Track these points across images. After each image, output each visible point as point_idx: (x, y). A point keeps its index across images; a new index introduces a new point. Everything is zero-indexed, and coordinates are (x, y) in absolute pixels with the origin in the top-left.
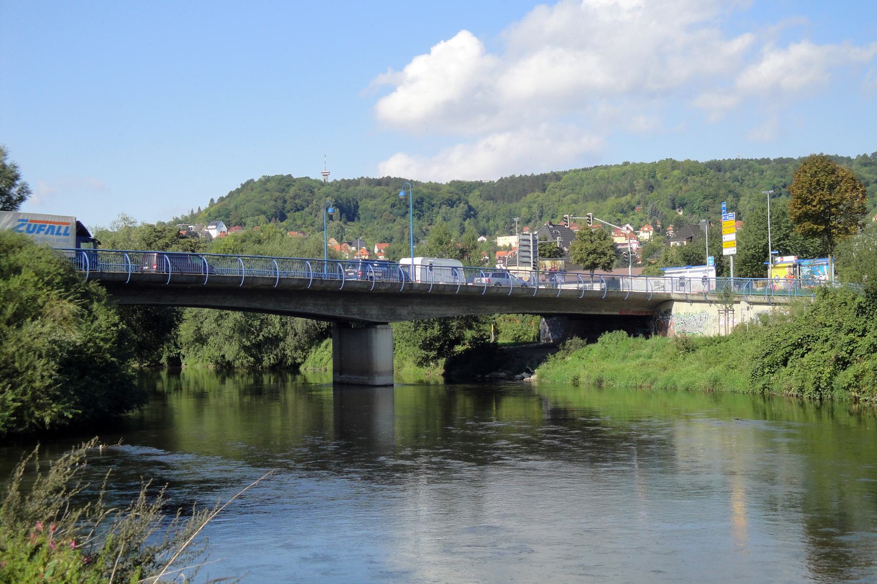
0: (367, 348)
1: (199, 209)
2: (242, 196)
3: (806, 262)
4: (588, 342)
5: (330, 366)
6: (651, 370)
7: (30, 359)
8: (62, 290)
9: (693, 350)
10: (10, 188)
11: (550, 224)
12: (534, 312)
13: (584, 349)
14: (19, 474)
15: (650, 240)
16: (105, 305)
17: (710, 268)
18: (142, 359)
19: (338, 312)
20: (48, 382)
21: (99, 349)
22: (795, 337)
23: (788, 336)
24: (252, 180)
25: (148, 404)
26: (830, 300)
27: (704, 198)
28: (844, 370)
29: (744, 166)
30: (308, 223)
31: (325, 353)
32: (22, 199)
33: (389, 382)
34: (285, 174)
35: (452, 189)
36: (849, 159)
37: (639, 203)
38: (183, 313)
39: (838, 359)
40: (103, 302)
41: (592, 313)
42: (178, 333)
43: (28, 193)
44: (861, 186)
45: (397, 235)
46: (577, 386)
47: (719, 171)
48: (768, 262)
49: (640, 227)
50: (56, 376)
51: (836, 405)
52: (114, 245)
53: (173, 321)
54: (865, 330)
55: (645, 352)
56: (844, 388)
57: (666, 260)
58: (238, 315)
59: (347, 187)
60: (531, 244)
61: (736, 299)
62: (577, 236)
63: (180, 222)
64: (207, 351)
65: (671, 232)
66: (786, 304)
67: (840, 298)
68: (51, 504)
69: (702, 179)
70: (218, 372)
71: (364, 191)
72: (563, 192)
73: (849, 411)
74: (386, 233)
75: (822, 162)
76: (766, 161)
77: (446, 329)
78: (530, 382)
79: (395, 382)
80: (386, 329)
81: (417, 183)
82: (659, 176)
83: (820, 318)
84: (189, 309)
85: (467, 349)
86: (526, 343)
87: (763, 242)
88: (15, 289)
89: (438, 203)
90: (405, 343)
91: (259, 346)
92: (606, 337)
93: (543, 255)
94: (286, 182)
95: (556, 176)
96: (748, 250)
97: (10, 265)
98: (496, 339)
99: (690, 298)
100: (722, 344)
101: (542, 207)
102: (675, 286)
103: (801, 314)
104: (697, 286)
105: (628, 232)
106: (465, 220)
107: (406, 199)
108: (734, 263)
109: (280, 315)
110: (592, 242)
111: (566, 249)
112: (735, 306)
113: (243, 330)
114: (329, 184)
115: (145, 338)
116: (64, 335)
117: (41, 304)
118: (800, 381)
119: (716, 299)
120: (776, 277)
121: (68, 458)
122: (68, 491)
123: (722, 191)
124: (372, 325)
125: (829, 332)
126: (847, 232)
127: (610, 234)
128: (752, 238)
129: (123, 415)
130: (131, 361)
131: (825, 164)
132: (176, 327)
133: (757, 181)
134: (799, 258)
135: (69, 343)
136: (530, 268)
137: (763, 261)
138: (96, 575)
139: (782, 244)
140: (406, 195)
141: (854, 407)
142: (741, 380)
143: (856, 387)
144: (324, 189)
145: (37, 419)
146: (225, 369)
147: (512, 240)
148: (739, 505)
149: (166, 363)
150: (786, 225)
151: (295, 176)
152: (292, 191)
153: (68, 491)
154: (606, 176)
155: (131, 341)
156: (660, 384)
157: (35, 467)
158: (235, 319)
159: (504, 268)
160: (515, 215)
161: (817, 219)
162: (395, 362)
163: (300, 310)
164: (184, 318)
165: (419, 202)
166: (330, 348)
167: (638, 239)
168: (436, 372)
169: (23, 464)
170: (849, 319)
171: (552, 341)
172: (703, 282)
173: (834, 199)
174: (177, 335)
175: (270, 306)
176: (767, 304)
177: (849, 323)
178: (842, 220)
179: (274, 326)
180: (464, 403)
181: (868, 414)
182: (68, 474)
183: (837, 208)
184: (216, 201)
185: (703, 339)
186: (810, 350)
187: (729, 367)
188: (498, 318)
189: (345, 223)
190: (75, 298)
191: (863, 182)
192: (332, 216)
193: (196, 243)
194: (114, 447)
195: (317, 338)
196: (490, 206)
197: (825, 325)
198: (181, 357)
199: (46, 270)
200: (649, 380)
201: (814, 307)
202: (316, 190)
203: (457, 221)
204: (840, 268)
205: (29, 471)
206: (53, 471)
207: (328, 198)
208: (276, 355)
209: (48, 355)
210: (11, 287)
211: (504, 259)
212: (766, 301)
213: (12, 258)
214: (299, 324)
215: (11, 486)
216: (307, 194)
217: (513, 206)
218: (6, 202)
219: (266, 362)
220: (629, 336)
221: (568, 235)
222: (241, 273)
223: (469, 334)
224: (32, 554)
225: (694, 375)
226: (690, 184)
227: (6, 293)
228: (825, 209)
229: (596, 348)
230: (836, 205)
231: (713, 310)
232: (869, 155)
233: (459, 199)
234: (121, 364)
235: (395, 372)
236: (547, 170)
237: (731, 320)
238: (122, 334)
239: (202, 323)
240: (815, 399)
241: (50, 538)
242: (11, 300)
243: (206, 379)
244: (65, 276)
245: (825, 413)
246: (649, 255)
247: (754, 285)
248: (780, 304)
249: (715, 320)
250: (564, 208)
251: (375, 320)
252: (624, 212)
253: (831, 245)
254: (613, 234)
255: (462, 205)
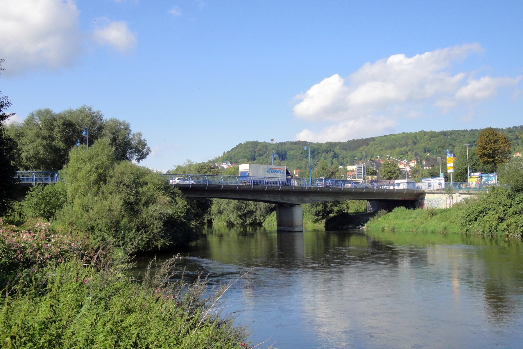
0: (291, 215)
1: (219, 156)
2: (237, 150)
3: (484, 175)
4: (388, 212)
5: (275, 223)
6: (416, 224)
7: (152, 221)
8: (164, 192)
9: (435, 215)
10: (143, 149)
11: (371, 160)
12: (364, 199)
13: (387, 215)
14: (149, 268)
15: (415, 166)
16: (181, 198)
17: (442, 178)
18: (196, 221)
19: (279, 200)
20: (159, 230)
21: (179, 216)
22: (480, 208)
23: (477, 208)
24: (241, 143)
25: (199, 239)
26: (496, 192)
27: (439, 148)
28: (502, 222)
29: (456, 133)
30: (265, 161)
31: (273, 217)
32: (148, 154)
33: (301, 230)
34: (255, 141)
35: (327, 146)
36: (502, 129)
37: (410, 150)
38: (212, 201)
39: (499, 218)
40: (180, 197)
41: (390, 199)
42: (211, 209)
43: (150, 151)
44: (508, 141)
45: (303, 166)
46: (384, 231)
47: (445, 135)
48: (468, 175)
49: (410, 161)
50: (162, 228)
51: (499, 238)
52: (184, 172)
53: (209, 204)
54: (511, 205)
55: (414, 216)
56: (502, 231)
57: (422, 175)
58: (236, 202)
59: (282, 146)
60: (362, 169)
61: (454, 192)
62: (383, 165)
63: (211, 162)
64: (223, 217)
65: (424, 163)
66: (476, 194)
67: (500, 191)
68: (163, 280)
69: (438, 139)
70: (228, 226)
71: (289, 147)
72: (376, 146)
73: (505, 240)
74: (299, 165)
75: (491, 131)
76: (466, 131)
77: (325, 206)
78: (363, 230)
79: (304, 230)
80: (300, 207)
81: (312, 143)
82: (418, 138)
83: (491, 200)
84: (215, 199)
85: (335, 215)
86: (360, 212)
87: (466, 167)
88: (145, 191)
89: (321, 152)
90: (307, 213)
91: (244, 215)
92: (396, 210)
93: (368, 174)
94: (255, 144)
95: (373, 139)
96: (459, 170)
97: (143, 181)
98: (348, 211)
99: (433, 192)
100: (448, 212)
101: (367, 153)
102: (426, 186)
103: (483, 198)
104: (436, 186)
105: (405, 163)
106: (333, 159)
107: (307, 150)
108: (452, 176)
109: (254, 201)
110: (389, 168)
111: (378, 171)
112: (453, 195)
113: (239, 208)
114: (274, 144)
115: (197, 212)
116: (165, 211)
117: (156, 198)
118: (483, 228)
119: (445, 192)
120: (472, 182)
121: (168, 262)
122: (168, 276)
123: (447, 144)
124: (294, 205)
125: (495, 206)
126: (503, 161)
127: (397, 164)
128: (460, 165)
129: (189, 244)
130: (192, 221)
131: (492, 132)
132: (210, 207)
133: (462, 140)
134: (481, 173)
135: (167, 214)
136: (362, 180)
137: (465, 175)
138: (182, 310)
139: (474, 167)
140: (307, 149)
141: (507, 238)
142: (456, 228)
143: (508, 230)
144: (272, 147)
145: (155, 245)
146: (231, 225)
147: (354, 168)
148: (456, 283)
149: (206, 222)
150: (475, 159)
151: (259, 142)
152: (258, 148)
153: (168, 276)
154: (395, 139)
155: (192, 213)
156: (420, 230)
157: (155, 265)
158: (235, 203)
159: (351, 180)
160: (355, 157)
161: (489, 156)
162: (304, 221)
163: (263, 199)
164: (213, 203)
165: (313, 152)
166: (276, 215)
167: (409, 166)
168: (321, 225)
169: (150, 264)
170: (504, 200)
171: (372, 212)
172: (439, 184)
173: (496, 147)
174: (211, 210)
175: (249, 197)
176: (468, 194)
177: (504, 202)
178: (500, 157)
179: (251, 206)
180: (334, 239)
181: (513, 242)
182: (169, 269)
183: (498, 151)
184: (226, 153)
185: (439, 210)
186: (487, 214)
187: (451, 222)
188: (348, 201)
189: (281, 161)
190: (169, 195)
191: (509, 139)
192: (275, 158)
193: (218, 171)
194: (188, 258)
195: (270, 211)
196: (344, 153)
197: (494, 203)
198: (212, 220)
199: (157, 183)
200: (415, 228)
201: (488, 195)
202: (268, 147)
203: (330, 159)
204: (500, 178)
205: (153, 267)
206: (162, 267)
207: (274, 151)
208: (252, 219)
209: (159, 219)
210: (144, 190)
211: (350, 176)
212: (467, 192)
213: (144, 178)
214: (262, 205)
215: (146, 273)
216: (264, 149)
217: (354, 152)
218: (141, 155)
219: (248, 222)
220: (407, 209)
221: (378, 165)
222: (237, 183)
223: (335, 209)
224: (156, 301)
225: (435, 226)
226: (433, 142)
227: (142, 193)
228: (493, 151)
229: (392, 214)
230: (497, 150)
231: (443, 197)
232: (511, 127)
233: (330, 150)
234: (188, 223)
235: (304, 226)
236: (369, 137)
237: (451, 201)
238: (188, 210)
239: (221, 205)
240: (489, 236)
241: (163, 295)
242: (144, 196)
243: (223, 229)
244: (165, 186)
245: (494, 242)
246: (415, 173)
247: (462, 186)
248: (473, 194)
249: (444, 201)
250: (377, 153)
251: (294, 203)
252: (403, 155)
253: (496, 167)
254: (398, 164)
255: (331, 152)
